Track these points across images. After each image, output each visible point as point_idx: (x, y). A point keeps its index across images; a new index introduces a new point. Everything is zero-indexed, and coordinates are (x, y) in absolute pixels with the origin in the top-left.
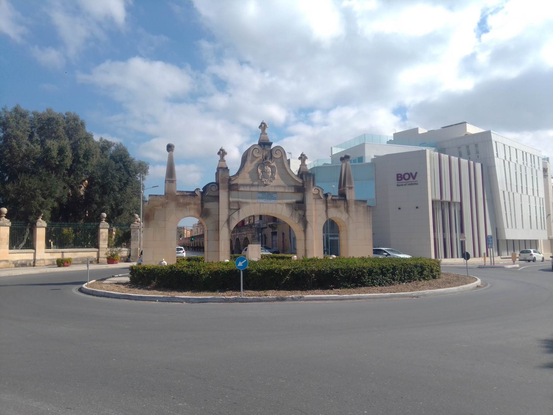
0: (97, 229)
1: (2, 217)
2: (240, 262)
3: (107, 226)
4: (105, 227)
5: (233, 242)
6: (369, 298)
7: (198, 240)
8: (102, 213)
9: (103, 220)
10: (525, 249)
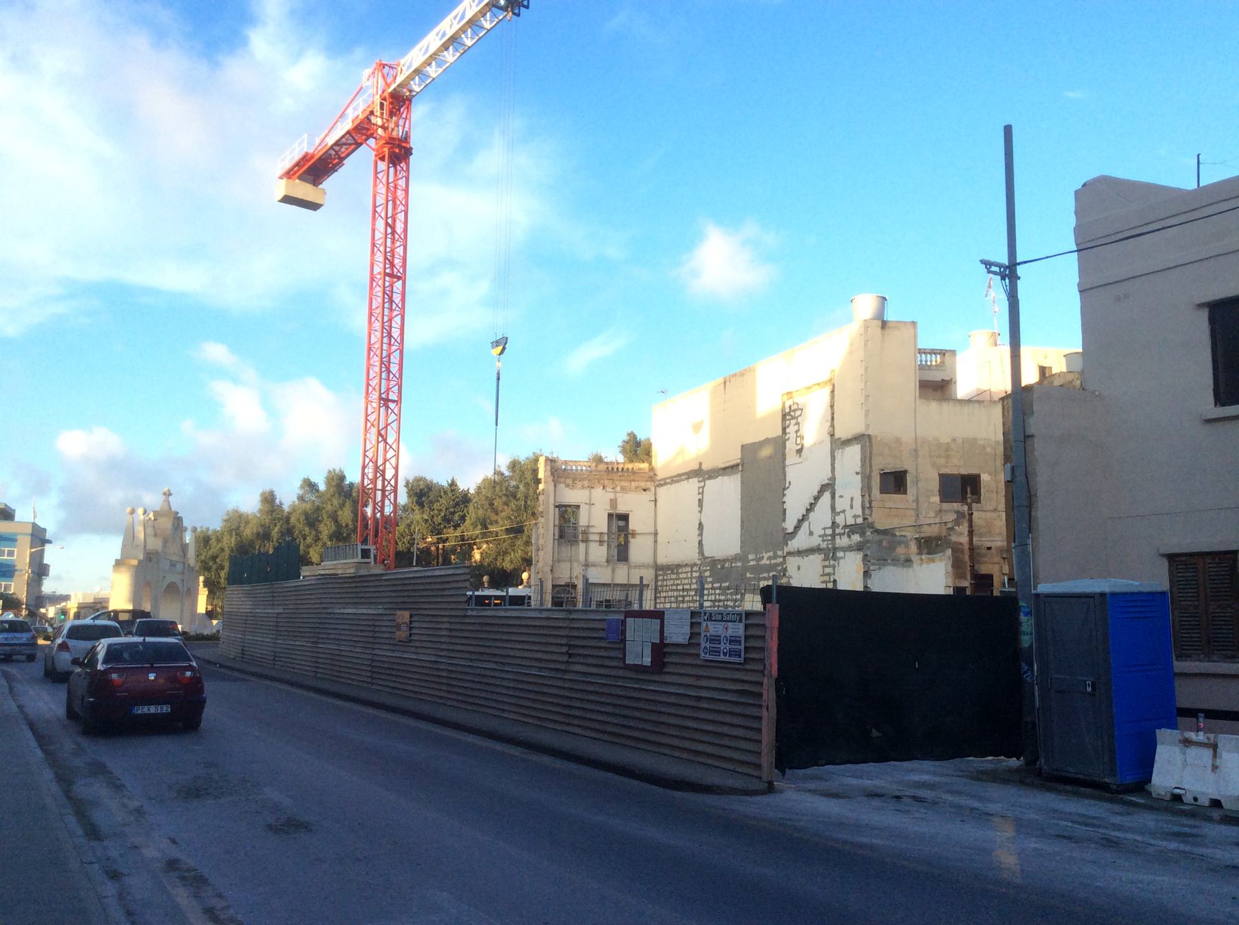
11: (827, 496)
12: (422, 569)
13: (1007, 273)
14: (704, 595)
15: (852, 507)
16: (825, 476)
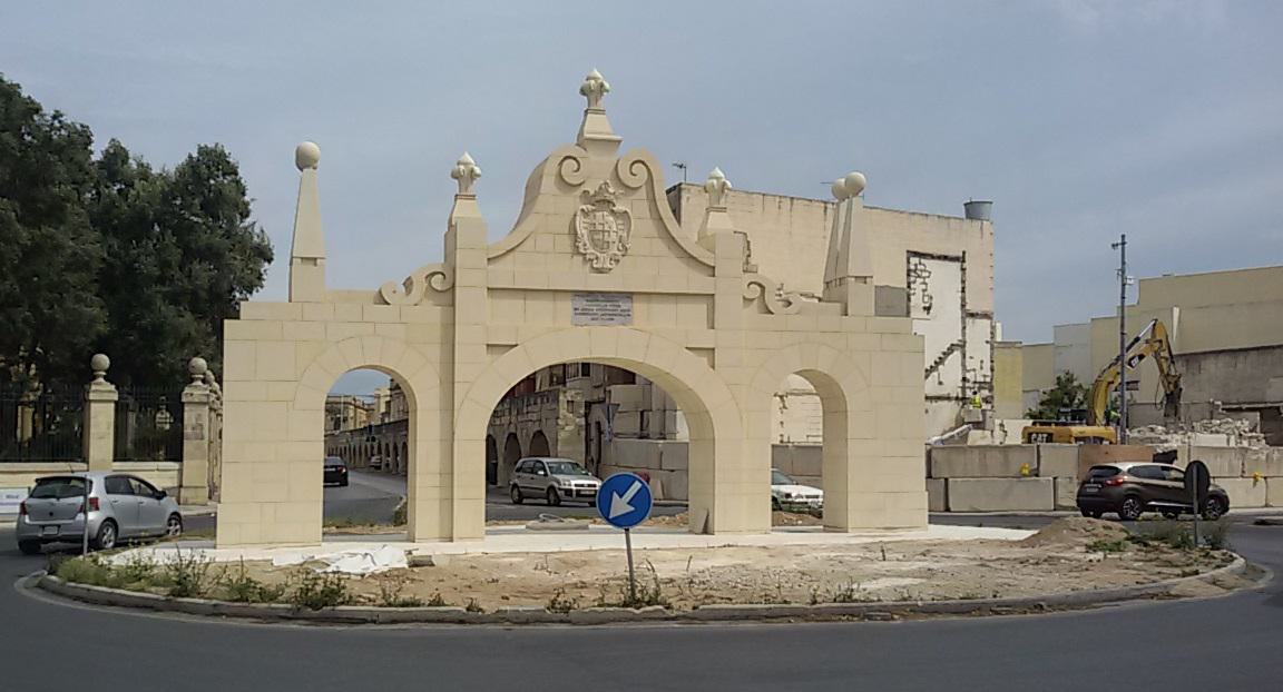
0: (82, 404)
1: (95, 378)
2: (615, 495)
3: (111, 395)
4: (106, 397)
5: (498, 446)
6: (1169, 501)
7: (391, 439)
8: (195, 359)
9: (99, 376)
10: (204, 487)
11: (957, 354)
12: (499, 561)
13: (32, 372)
14: (23, 134)
15: (982, 368)
16: (956, 338)
